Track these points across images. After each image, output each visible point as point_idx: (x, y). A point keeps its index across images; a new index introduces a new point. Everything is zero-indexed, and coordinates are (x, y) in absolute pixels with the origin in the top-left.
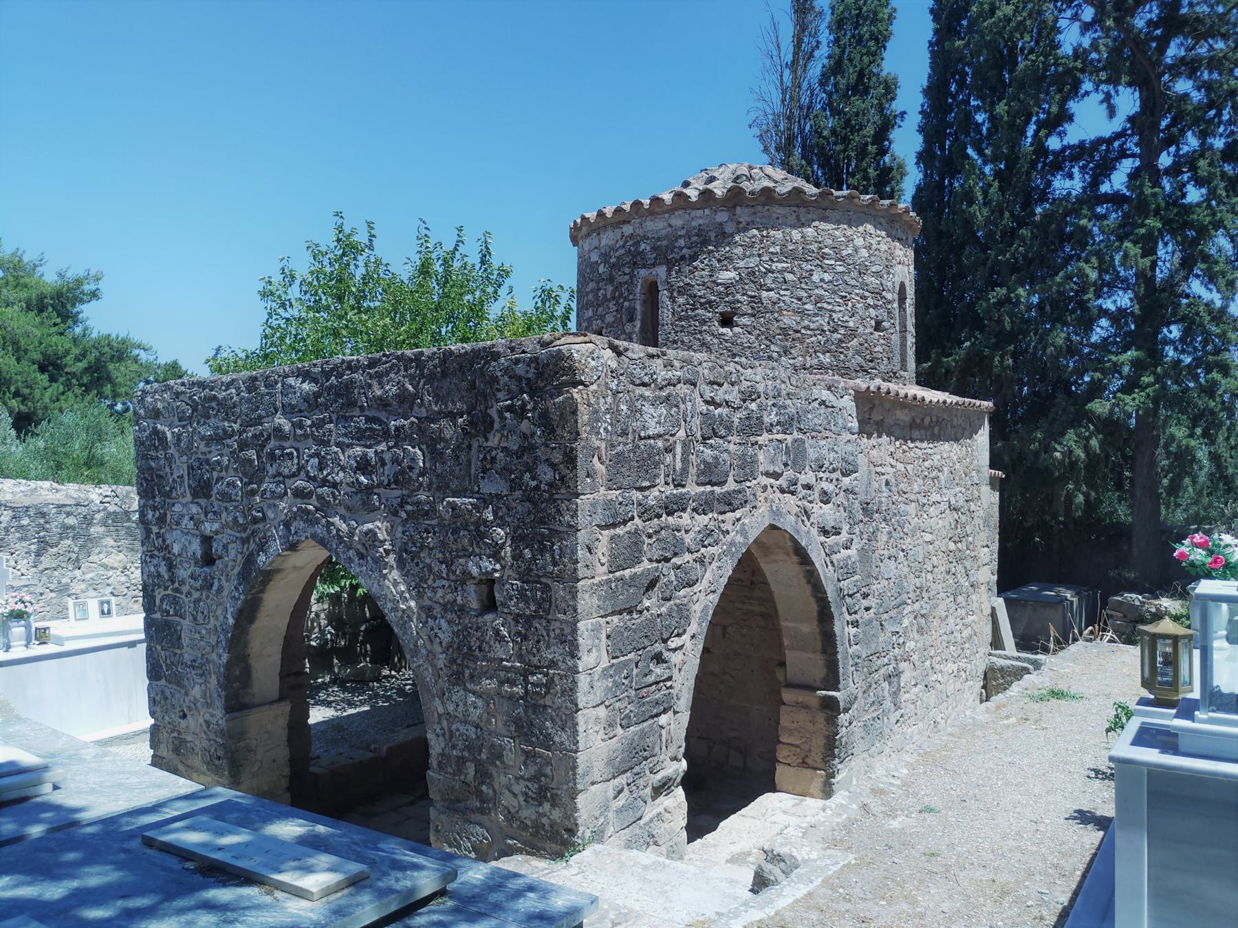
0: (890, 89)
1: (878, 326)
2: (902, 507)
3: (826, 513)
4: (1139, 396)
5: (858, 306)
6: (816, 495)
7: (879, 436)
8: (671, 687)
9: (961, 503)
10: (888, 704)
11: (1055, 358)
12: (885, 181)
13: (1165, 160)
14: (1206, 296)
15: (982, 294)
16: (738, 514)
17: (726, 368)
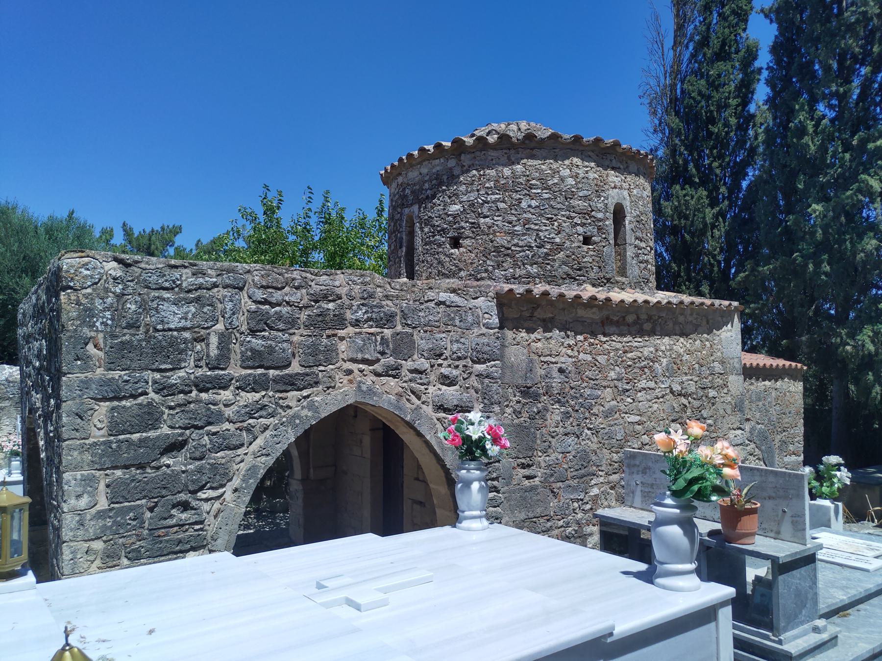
0: (752, 54)
1: (587, 240)
3: (451, 394)
5: (564, 224)
6: (433, 377)
8: (201, 529)
16: (305, 393)
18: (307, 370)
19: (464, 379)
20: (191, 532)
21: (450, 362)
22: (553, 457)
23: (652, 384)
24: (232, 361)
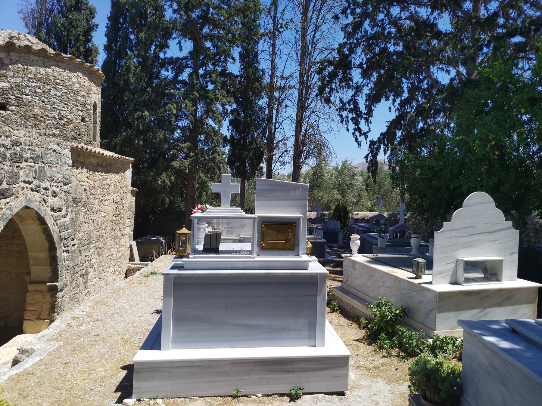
1: (83, 120)
2: (92, 201)
3: (55, 202)
4: (189, 160)
5: (73, 109)
6: (50, 193)
7: (82, 169)
9: (119, 200)
10: (82, 287)
11: (160, 143)
12: (89, 54)
13: (201, 72)
14: (213, 125)
15: (131, 113)
16: (8, 200)
17: (4, 129)
23: (109, 197)
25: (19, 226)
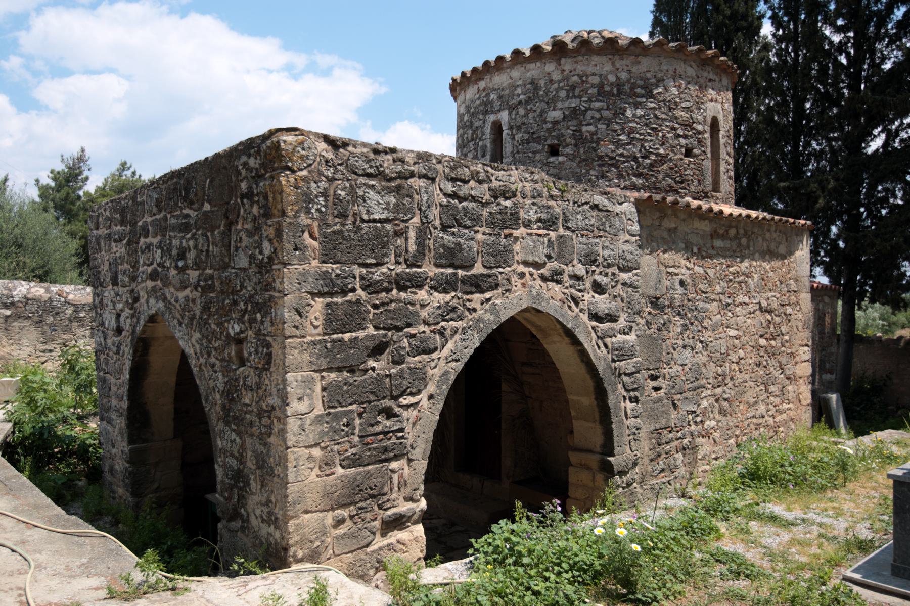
1: (688, 153)
3: (603, 303)
5: (668, 135)
6: (588, 284)
8: (402, 437)
10: (682, 471)
16: (488, 295)
18: (489, 271)
19: (613, 287)
20: (394, 440)
21: (601, 269)
22: (674, 370)
23: (746, 300)
24: (427, 258)
25: (545, 346)
